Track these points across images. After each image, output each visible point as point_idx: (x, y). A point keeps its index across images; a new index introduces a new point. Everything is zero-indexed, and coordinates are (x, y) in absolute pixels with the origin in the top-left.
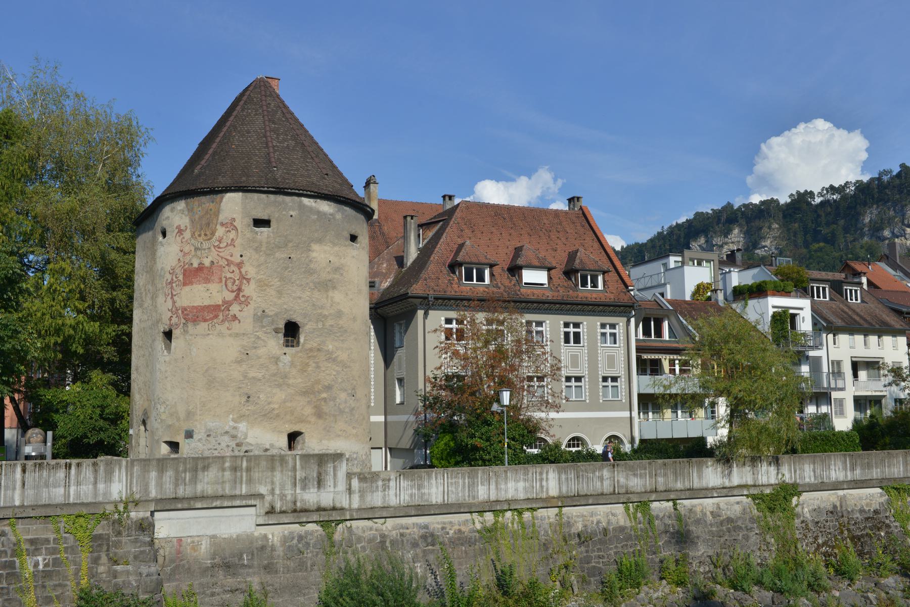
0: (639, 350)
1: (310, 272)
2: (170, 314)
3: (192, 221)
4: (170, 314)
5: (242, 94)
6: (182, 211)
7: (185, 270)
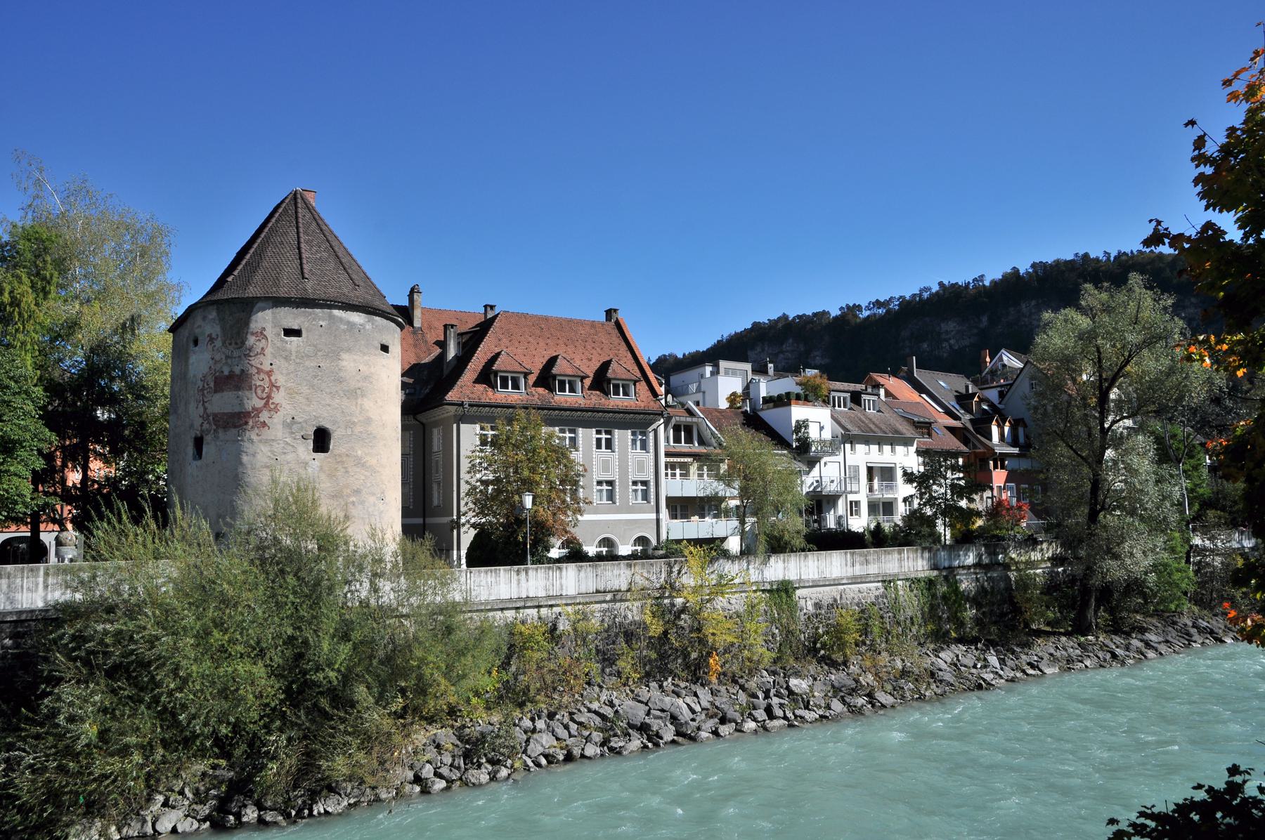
0: (668, 455)
1: (340, 381)
2: (201, 420)
3: (223, 329)
4: (201, 420)
5: (278, 206)
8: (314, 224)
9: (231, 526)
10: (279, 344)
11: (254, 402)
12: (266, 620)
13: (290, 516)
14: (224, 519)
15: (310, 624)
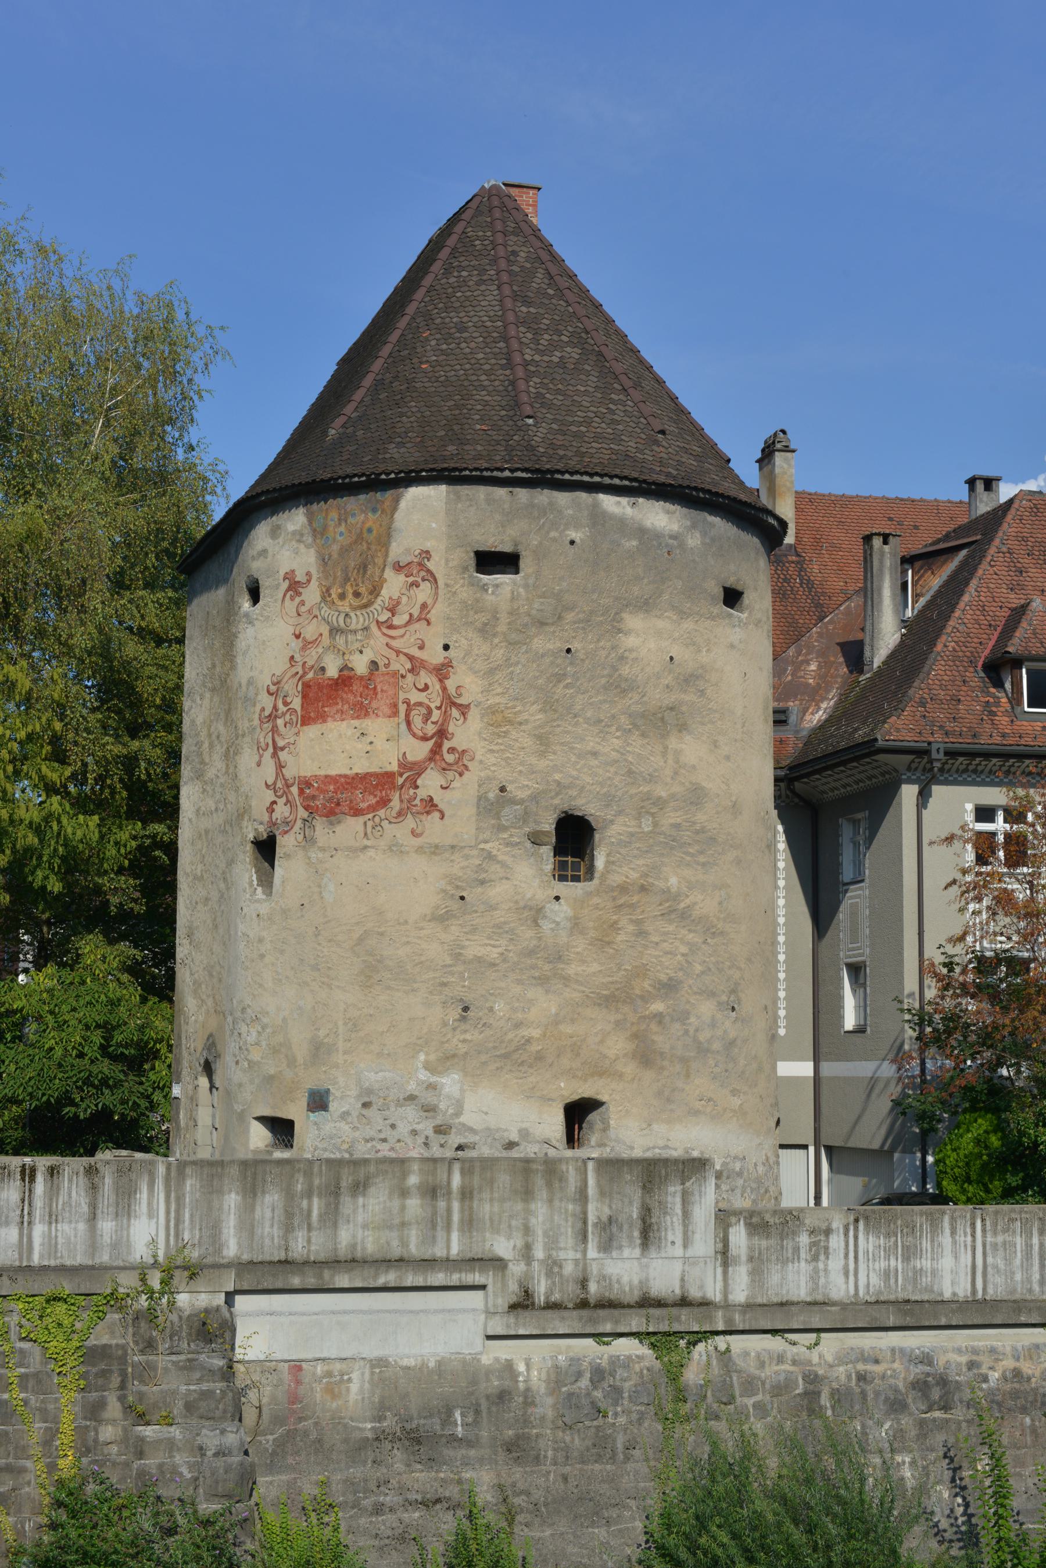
3: (324, 561)
4: (270, 796)
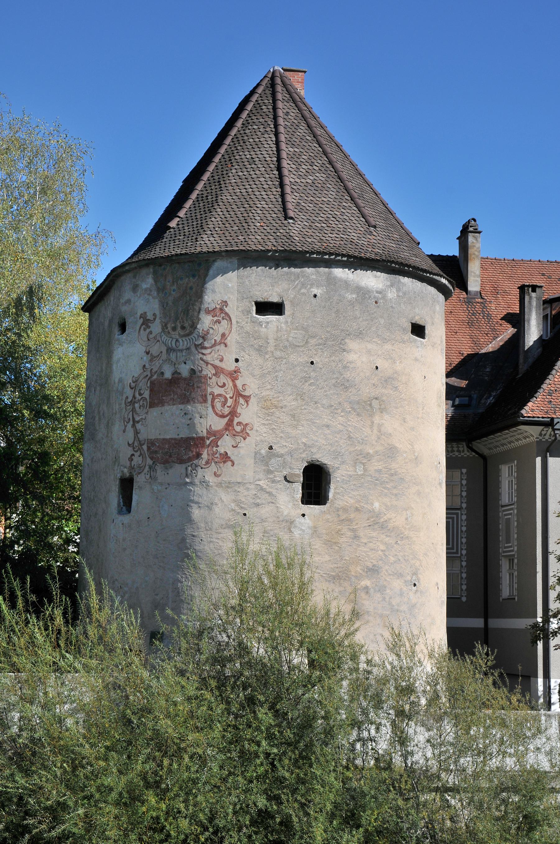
1: (345, 385)
2: (130, 451)
3: (163, 305)
4: (130, 451)
6: (148, 291)
7: (152, 383)
8: (303, 126)
9: (173, 622)
10: (248, 327)
11: (208, 421)
12: (224, 780)
13: (265, 610)
14: (163, 610)
15: (294, 791)
